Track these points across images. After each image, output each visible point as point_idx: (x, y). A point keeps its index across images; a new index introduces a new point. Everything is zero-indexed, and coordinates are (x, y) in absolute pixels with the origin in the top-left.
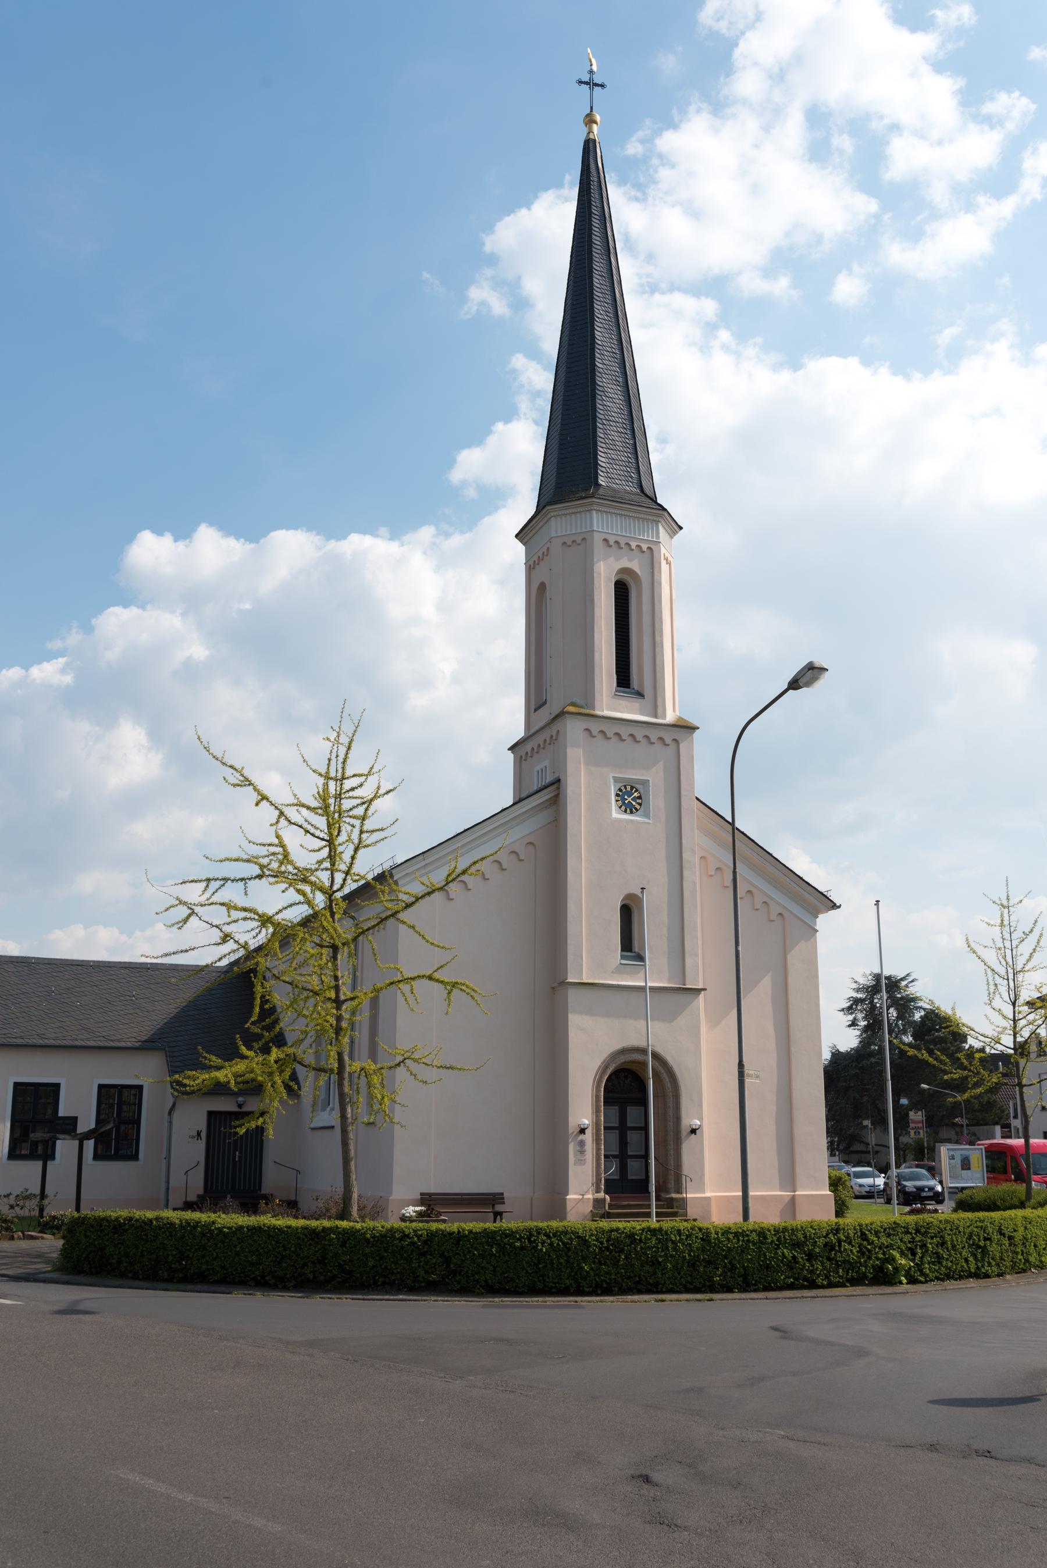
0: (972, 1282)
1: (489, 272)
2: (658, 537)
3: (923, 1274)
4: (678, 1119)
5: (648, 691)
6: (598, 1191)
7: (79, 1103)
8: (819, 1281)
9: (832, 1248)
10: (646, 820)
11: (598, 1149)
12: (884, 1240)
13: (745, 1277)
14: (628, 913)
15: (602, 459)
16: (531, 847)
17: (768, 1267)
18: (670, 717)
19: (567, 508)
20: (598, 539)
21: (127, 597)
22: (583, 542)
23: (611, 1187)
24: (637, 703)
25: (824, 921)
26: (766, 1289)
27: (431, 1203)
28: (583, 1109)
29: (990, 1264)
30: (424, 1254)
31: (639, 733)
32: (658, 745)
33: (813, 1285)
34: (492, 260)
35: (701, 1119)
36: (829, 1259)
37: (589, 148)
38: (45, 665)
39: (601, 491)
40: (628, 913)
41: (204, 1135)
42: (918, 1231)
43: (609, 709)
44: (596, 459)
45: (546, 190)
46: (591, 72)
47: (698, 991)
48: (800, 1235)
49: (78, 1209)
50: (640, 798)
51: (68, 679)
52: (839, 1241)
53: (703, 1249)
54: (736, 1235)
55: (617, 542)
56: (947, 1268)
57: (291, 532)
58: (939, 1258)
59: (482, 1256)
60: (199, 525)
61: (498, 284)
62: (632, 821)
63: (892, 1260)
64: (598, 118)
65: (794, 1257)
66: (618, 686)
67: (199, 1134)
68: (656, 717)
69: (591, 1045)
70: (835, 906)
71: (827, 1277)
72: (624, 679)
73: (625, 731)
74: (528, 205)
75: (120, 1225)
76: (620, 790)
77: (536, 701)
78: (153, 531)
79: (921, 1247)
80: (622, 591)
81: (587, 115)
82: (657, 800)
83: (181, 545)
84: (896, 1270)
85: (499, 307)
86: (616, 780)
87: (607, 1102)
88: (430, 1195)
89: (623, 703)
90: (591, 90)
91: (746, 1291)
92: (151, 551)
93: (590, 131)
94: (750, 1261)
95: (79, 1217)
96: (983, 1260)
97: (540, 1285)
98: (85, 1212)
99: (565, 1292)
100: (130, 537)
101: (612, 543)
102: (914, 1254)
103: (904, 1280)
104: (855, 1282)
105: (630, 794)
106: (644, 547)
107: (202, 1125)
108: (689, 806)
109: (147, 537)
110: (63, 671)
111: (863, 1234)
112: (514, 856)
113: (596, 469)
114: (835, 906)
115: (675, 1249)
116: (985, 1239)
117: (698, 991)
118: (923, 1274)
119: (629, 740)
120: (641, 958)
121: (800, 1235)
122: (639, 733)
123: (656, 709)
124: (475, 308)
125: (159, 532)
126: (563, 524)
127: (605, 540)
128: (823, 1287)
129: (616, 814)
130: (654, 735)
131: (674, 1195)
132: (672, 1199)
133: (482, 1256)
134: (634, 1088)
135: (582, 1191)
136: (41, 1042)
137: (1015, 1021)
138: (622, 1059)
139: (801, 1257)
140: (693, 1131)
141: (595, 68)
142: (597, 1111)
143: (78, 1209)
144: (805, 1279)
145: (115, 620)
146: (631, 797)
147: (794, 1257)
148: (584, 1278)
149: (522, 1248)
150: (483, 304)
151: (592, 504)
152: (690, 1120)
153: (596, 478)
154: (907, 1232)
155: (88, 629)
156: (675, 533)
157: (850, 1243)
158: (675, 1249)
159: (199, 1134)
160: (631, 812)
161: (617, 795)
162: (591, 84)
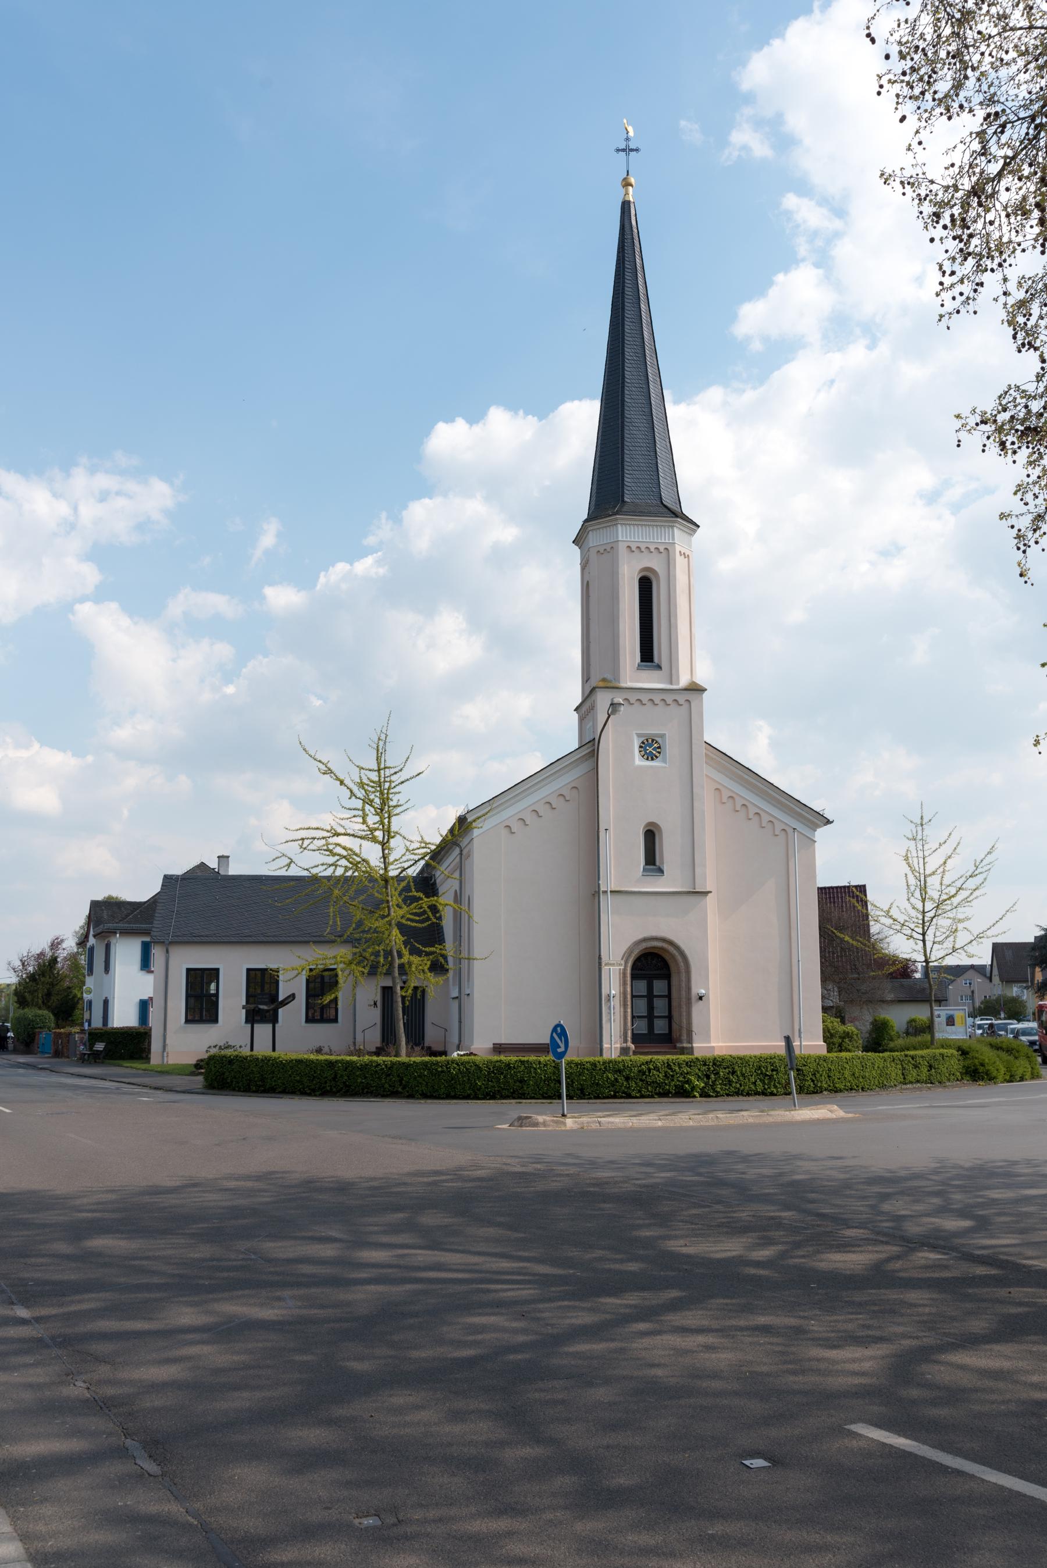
0: (761, 1097)
1: (748, 111)
2: (673, 539)
3: (714, 1091)
4: (689, 989)
5: (664, 664)
6: (625, 1041)
7: (292, 984)
8: (633, 1094)
9: (644, 1073)
10: (664, 765)
11: (625, 1012)
12: (686, 1069)
13: (582, 1090)
14: (651, 836)
15: (627, 480)
16: (574, 790)
17: (598, 1084)
18: (684, 681)
19: (599, 523)
20: (622, 548)
21: (424, 489)
22: (610, 550)
23: (636, 1038)
24: (656, 673)
25: (821, 834)
26: (597, 1097)
27: (499, 1049)
28: (614, 981)
29: (775, 1087)
30: (389, 1075)
31: (657, 698)
32: (673, 706)
33: (629, 1096)
34: (749, 98)
35: (707, 989)
36: (641, 1080)
37: (626, 206)
38: (498, 418)
39: (625, 509)
40: (651, 836)
41: (379, 1004)
42: (714, 1064)
43: (631, 681)
44: (623, 480)
45: (796, 18)
46: (627, 139)
47: (706, 893)
48: (621, 1065)
49: (252, 1049)
50: (659, 747)
51: (382, 571)
52: (649, 1070)
53: (554, 1073)
54: (577, 1064)
55: (638, 547)
56: (735, 1088)
57: (576, 403)
58: (730, 1082)
59: (420, 1076)
60: (488, 408)
61: (759, 123)
62: (652, 767)
63: (688, 1082)
64: (632, 180)
65: (616, 1079)
66: (642, 661)
67: (375, 1004)
68: (671, 684)
69: (620, 936)
70: (828, 822)
71: (640, 1091)
72: (647, 654)
73: (645, 697)
74: (781, 35)
75: (284, 1065)
76: (643, 743)
77: (586, 678)
78: (446, 422)
79: (715, 1074)
80: (646, 586)
81: (625, 179)
82: (672, 748)
83: (477, 429)
84: (693, 1088)
85: (760, 149)
86: (639, 735)
87: (634, 977)
88: (500, 1045)
89: (646, 674)
90: (628, 155)
91: (582, 1099)
92: (449, 438)
93: (627, 194)
94: (585, 1080)
95: (251, 1056)
96: (769, 1084)
97: (453, 1094)
98: (254, 1053)
99: (467, 1097)
100: (427, 431)
101: (634, 549)
102: (708, 1077)
103: (697, 1094)
104: (662, 1095)
105: (650, 746)
106: (662, 549)
107: (378, 998)
108: (699, 751)
109: (441, 427)
110: (379, 562)
111: (669, 1065)
112: (561, 798)
113: (623, 487)
114: (828, 822)
115: (536, 1073)
116: (773, 1070)
117: (706, 893)
118: (714, 1091)
119: (649, 704)
120: (661, 871)
121: (621, 1065)
122: (657, 698)
123: (671, 678)
124: (736, 154)
125: (449, 420)
126: (596, 539)
127: (629, 547)
128: (636, 1097)
129: (639, 761)
130: (669, 698)
131: (685, 1045)
132: (683, 1048)
133: (420, 1076)
134: (657, 969)
135: (614, 1042)
136: (264, 939)
137: (924, 912)
138: (644, 945)
139: (621, 1079)
140: (701, 998)
141: (631, 134)
142: (625, 984)
143: (252, 1049)
144: (624, 1092)
145: (420, 512)
146: (651, 748)
147: (616, 1079)
148: (479, 1090)
149: (442, 1072)
150: (745, 148)
151: (616, 519)
152: (697, 989)
153: (623, 496)
154: (705, 1065)
155: (396, 519)
156: (695, 531)
157: (658, 1071)
158: (536, 1073)
159: (375, 1004)
160: (652, 759)
161: (641, 747)
162: (627, 150)
